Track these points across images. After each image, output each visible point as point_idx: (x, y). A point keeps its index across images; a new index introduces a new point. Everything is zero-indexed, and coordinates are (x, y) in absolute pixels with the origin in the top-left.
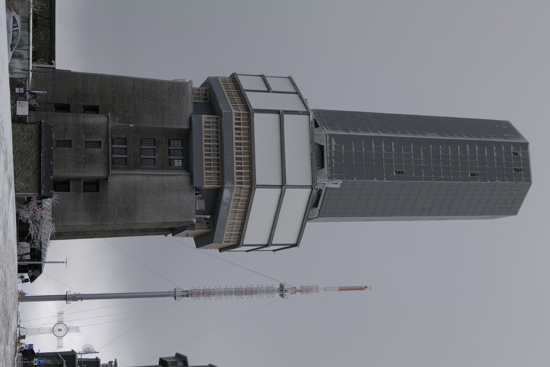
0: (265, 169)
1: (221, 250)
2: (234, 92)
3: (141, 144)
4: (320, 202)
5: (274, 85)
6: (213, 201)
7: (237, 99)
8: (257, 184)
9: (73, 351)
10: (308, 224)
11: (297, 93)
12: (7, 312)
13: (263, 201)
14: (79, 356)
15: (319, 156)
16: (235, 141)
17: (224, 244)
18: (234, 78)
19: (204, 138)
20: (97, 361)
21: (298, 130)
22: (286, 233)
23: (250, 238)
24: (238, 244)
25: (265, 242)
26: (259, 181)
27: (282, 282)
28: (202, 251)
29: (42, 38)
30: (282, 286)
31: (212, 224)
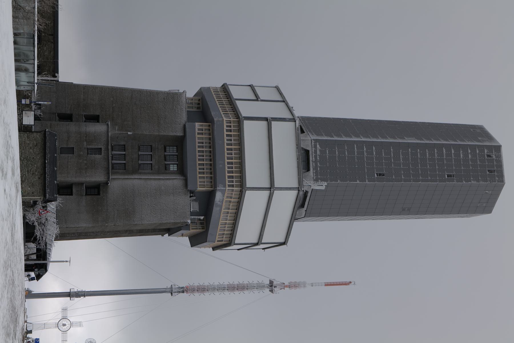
0: (255, 172)
1: (214, 249)
2: (225, 101)
6: (207, 203)
7: (228, 107)
10: (296, 224)
11: (284, 101)
13: (253, 203)
17: (217, 243)
18: (225, 88)
21: (284, 135)
22: (274, 232)
23: (239, 238)
24: (230, 242)
26: (249, 184)
27: (272, 278)
28: (195, 249)
30: (271, 282)
31: (206, 224)
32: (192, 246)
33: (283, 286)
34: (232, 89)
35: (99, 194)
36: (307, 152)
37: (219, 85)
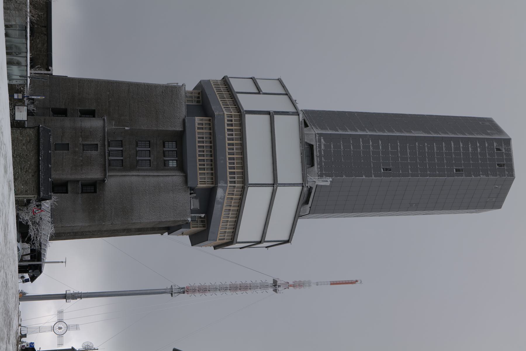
0: (258, 168)
1: (215, 247)
2: (226, 94)
3: (137, 146)
5: (264, 87)
7: (229, 101)
8: (250, 182)
10: (300, 221)
11: (287, 94)
12: (9, 312)
13: (256, 199)
15: (309, 155)
17: (218, 242)
18: (225, 81)
19: (197, 140)
21: (288, 129)
22: (278, 230)
23: (241, 236)
24: (232, 242)
26: (251, 180)
27: (276, 278)
28: (196, 248)
31: (207, 222)
35: (95, 192)
36: (311, 147)
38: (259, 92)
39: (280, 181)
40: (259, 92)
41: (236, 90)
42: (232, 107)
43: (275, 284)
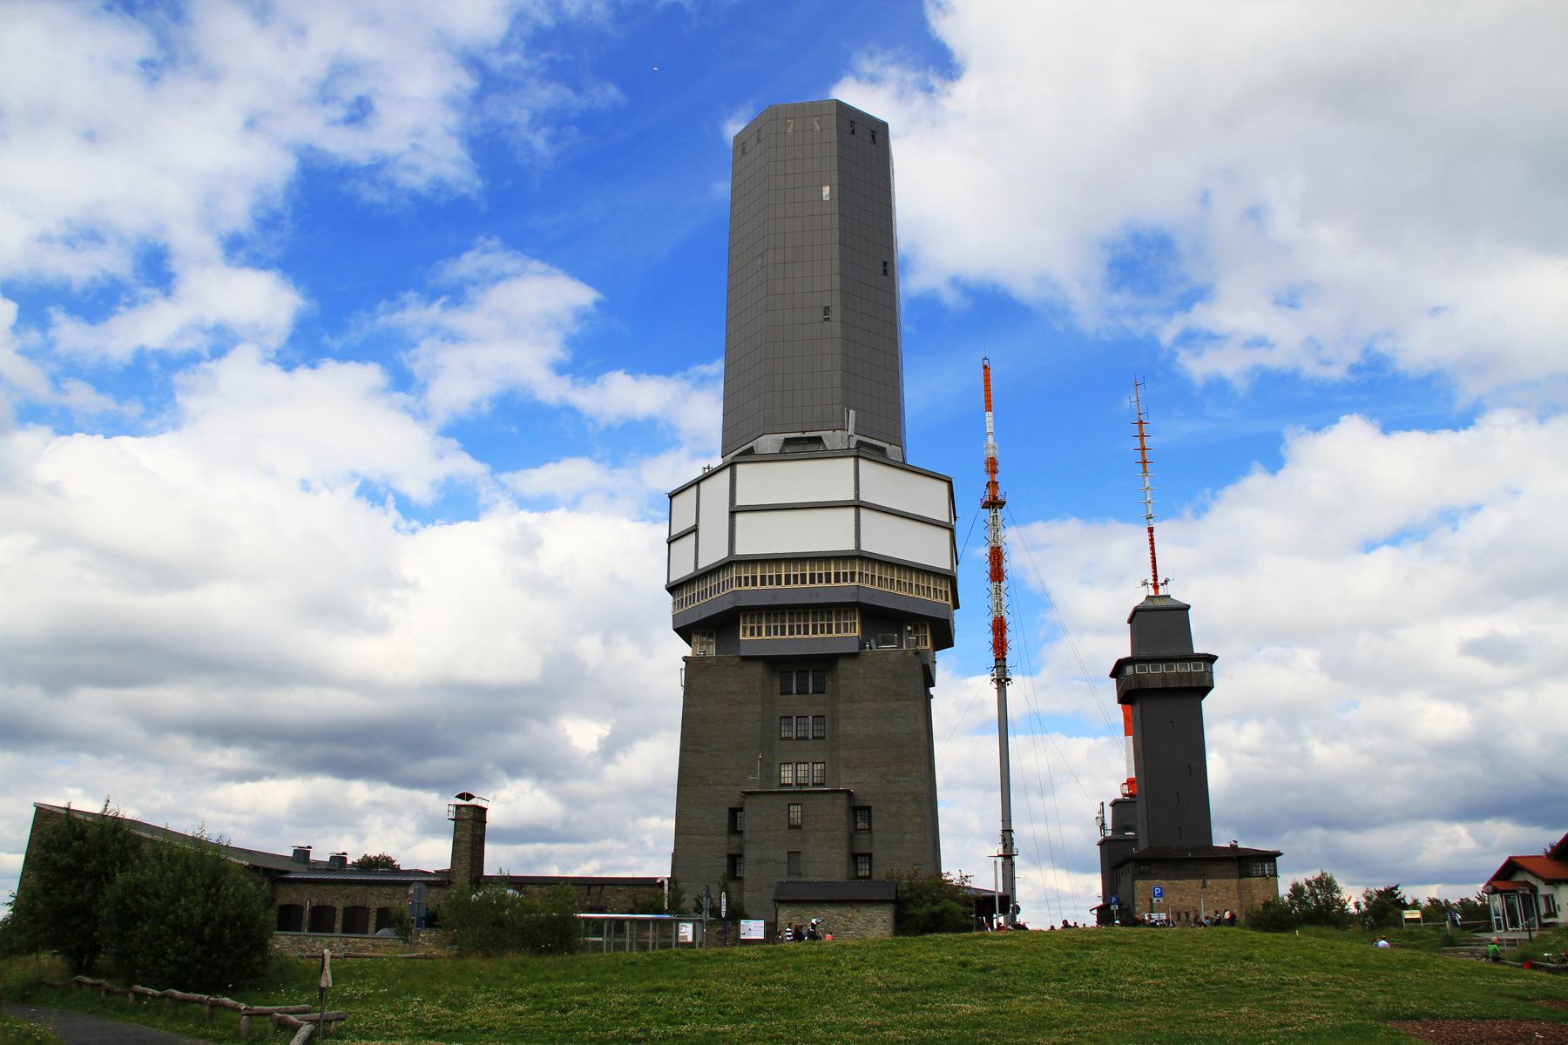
0: (833, 534)
1: (956, 606)
2: (699, 588)
3: (806, 738)
4: (874, 442)
5: (683, 522)
6: (882, 620)
7: (711, 583)
8: (852, 547)
9: (1101, 844)
11: (697, 482)
12: (1397, 1014)
13: (885, 538)
14: (1109, 834)
15: (803, 447)
16: (832, 583)
18: (672, 589)
19: (756, 637)
20: (1115, 804)
21: (757, 483)
22: (930, 499)
25: (947, 533)
26: (848, 545)
27: (979, 505)
29: (620, 897)
30: (987, 505)
31: (917, 621)
32: (952, 645)
33: (993, 485)
34: (675, 578)
35: (869, 809)
36: (787, 442)
37: (1114, 680)
38: (695, 530)
39: (851, 497)
40: (695, 530)
41: (692, 570)
42: (724, 577)
43: (994, 504)
